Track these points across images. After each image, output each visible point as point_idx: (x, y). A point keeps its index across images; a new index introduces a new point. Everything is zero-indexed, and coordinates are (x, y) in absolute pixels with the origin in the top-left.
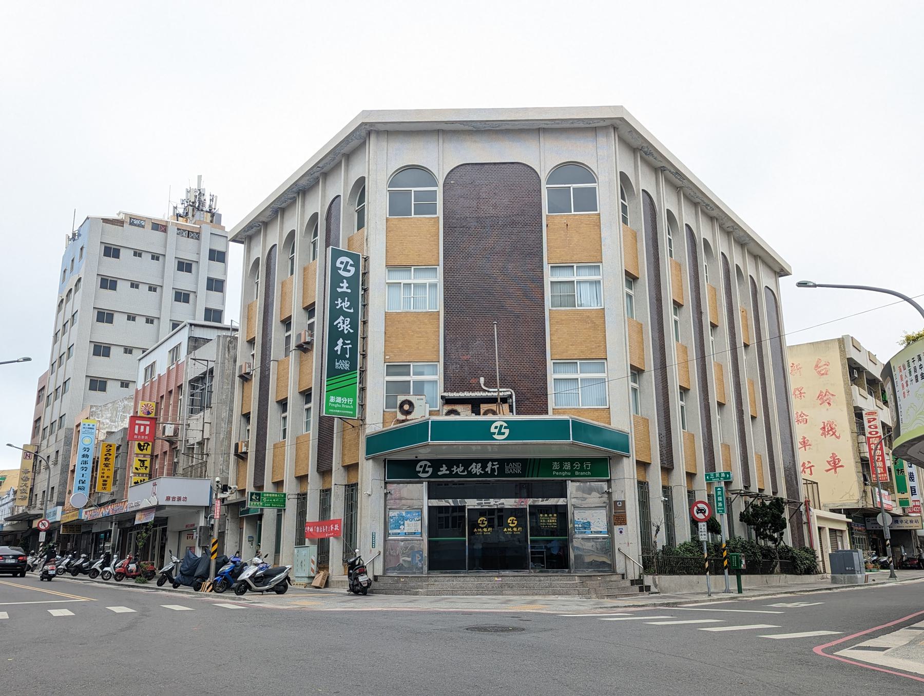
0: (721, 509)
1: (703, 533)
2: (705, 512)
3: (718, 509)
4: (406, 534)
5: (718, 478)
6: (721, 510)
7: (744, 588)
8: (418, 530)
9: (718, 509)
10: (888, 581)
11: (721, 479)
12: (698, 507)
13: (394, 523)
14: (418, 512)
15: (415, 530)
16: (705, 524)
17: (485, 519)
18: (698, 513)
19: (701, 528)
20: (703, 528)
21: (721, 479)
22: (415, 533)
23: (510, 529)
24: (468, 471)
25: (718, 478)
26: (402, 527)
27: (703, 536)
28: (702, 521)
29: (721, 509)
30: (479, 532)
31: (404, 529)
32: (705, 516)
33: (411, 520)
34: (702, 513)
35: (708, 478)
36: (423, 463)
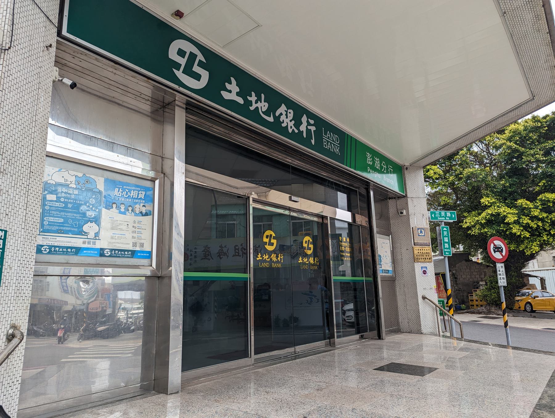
0: (447, 250)
1: (502, 277)
2: (502, 251)
3: (445, 250)
4: (102, 255)
5: (443, 217)
6: (447, 252)
7: (100, 273)
8: (142, 245)
9: (445, 250)
10: (497, 316)
11: (447, 218)
12: (495, 245)
13: (58, 209)
14: (146, 189)
15: (135, 244)
16: (503, 265)
17: (274, 235)
18: (495, 252)
19: (499, 271)
20: (501, 270)
21: (447, 218)
22: (133, 254)
23: (266, 257)
24: (275, 117)
25: (443, 217)
26: (90, 228)
27: (502, 280)
28: (500, 261)
29: (447, 250)
30: (265, 261)
31: (97, 234)
32: (502, 255)
33: (123, 208)
34: (499, 251)
35: (433, 215)
36: (189, 48)
